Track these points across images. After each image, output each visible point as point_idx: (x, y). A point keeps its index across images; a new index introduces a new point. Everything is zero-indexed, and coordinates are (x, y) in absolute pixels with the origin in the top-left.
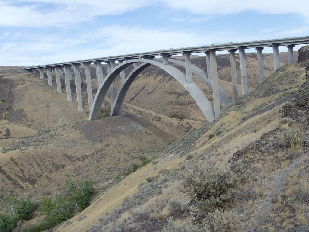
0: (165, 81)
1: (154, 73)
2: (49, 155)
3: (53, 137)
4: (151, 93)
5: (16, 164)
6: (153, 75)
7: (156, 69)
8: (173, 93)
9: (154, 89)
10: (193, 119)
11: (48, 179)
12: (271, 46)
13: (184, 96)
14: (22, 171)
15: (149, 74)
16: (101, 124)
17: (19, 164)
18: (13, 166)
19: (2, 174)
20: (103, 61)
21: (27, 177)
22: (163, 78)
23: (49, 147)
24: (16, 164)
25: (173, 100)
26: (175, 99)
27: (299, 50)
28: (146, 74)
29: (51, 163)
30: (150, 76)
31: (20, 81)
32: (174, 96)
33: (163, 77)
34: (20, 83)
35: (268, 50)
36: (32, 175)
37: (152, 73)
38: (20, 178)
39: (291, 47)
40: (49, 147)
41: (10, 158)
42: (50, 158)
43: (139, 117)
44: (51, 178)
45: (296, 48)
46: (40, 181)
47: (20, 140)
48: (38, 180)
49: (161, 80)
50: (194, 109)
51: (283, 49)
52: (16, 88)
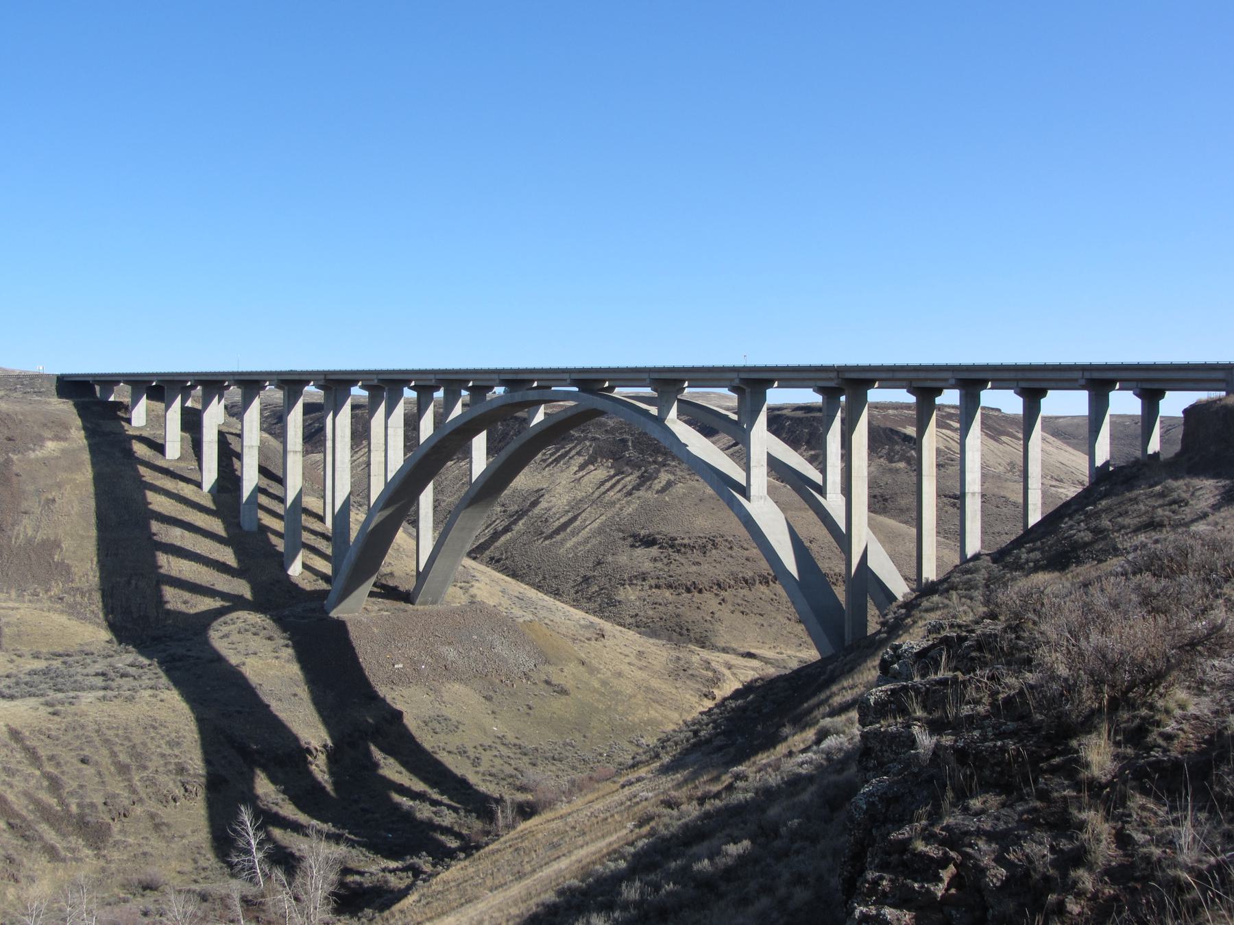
0: (619, 487)
1: (579, 454)
2: (163, 731)
3: (178, 664)
4: (557, 531)
5: (33, 756)
6: (572, 461)
7: (586, 438)
8: (649, 542)
9: (574, 519)
10: (725, 650)
11: (157, 827)
12: (1082, 388)
13: (696, 555)
14: (55, 785)
15: (552, 455)
16: (375, 630)
17: (43, 753)
18: (19, 762)
19: (272, 708)
20: (354, 383)
21: (74, 809)
22: (611, 477)
23: (162, 701)
24: (33, 756)
25: (647, 566)
26: (659, 565)
27: (1185, 411)
28: (544, 454)
29: (172, 767)
30: (557, 461)
31: (48, 428)
32: (654, 551)
33: (612, 472)
34: (47, 434)
35: (1124, 403)
36: (92, 805)
37: (567, 453)
38: (45, 813)
39: (1151, 398)
40: (162, 701)
41: (5, 729)
42: (168, 743)
43: (521, 620)
44: (168, 825)
45: (1174, 404)
46: (122, 831)
47: (40, 665)
48: (116, 827)
49: (602, 483)
50: (733, 612)
51: (1124, 403)
52: (32, 455)
